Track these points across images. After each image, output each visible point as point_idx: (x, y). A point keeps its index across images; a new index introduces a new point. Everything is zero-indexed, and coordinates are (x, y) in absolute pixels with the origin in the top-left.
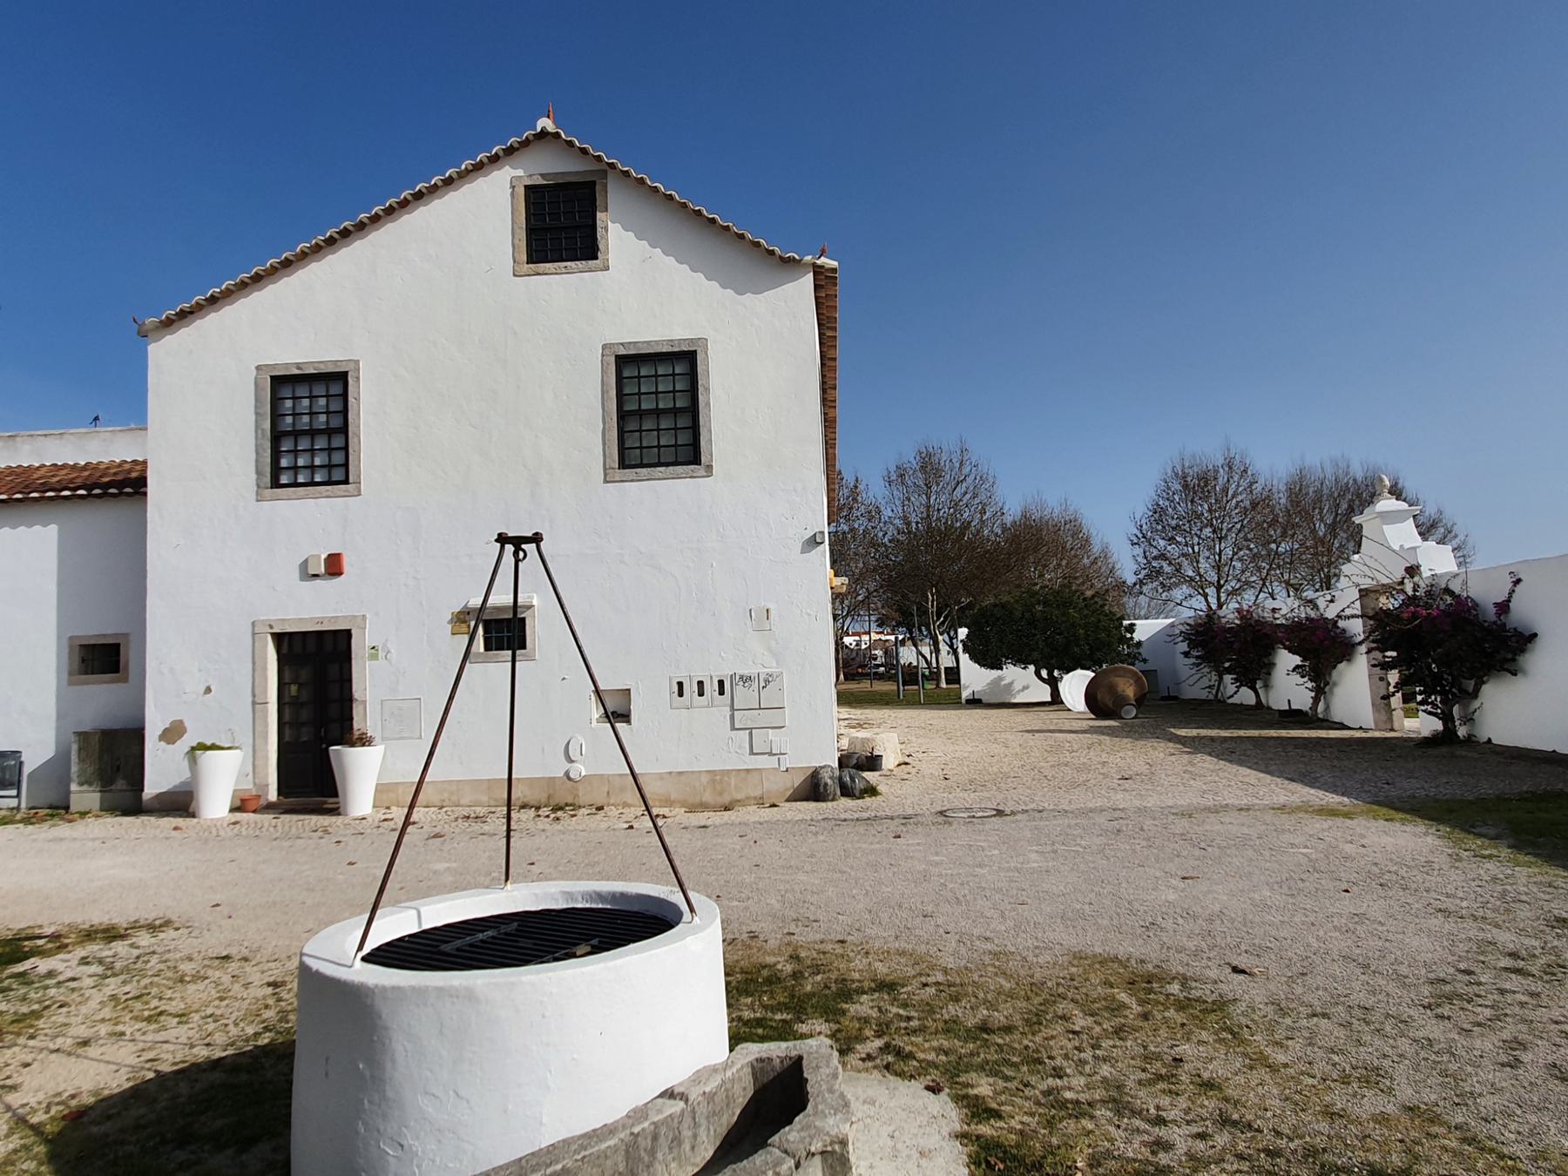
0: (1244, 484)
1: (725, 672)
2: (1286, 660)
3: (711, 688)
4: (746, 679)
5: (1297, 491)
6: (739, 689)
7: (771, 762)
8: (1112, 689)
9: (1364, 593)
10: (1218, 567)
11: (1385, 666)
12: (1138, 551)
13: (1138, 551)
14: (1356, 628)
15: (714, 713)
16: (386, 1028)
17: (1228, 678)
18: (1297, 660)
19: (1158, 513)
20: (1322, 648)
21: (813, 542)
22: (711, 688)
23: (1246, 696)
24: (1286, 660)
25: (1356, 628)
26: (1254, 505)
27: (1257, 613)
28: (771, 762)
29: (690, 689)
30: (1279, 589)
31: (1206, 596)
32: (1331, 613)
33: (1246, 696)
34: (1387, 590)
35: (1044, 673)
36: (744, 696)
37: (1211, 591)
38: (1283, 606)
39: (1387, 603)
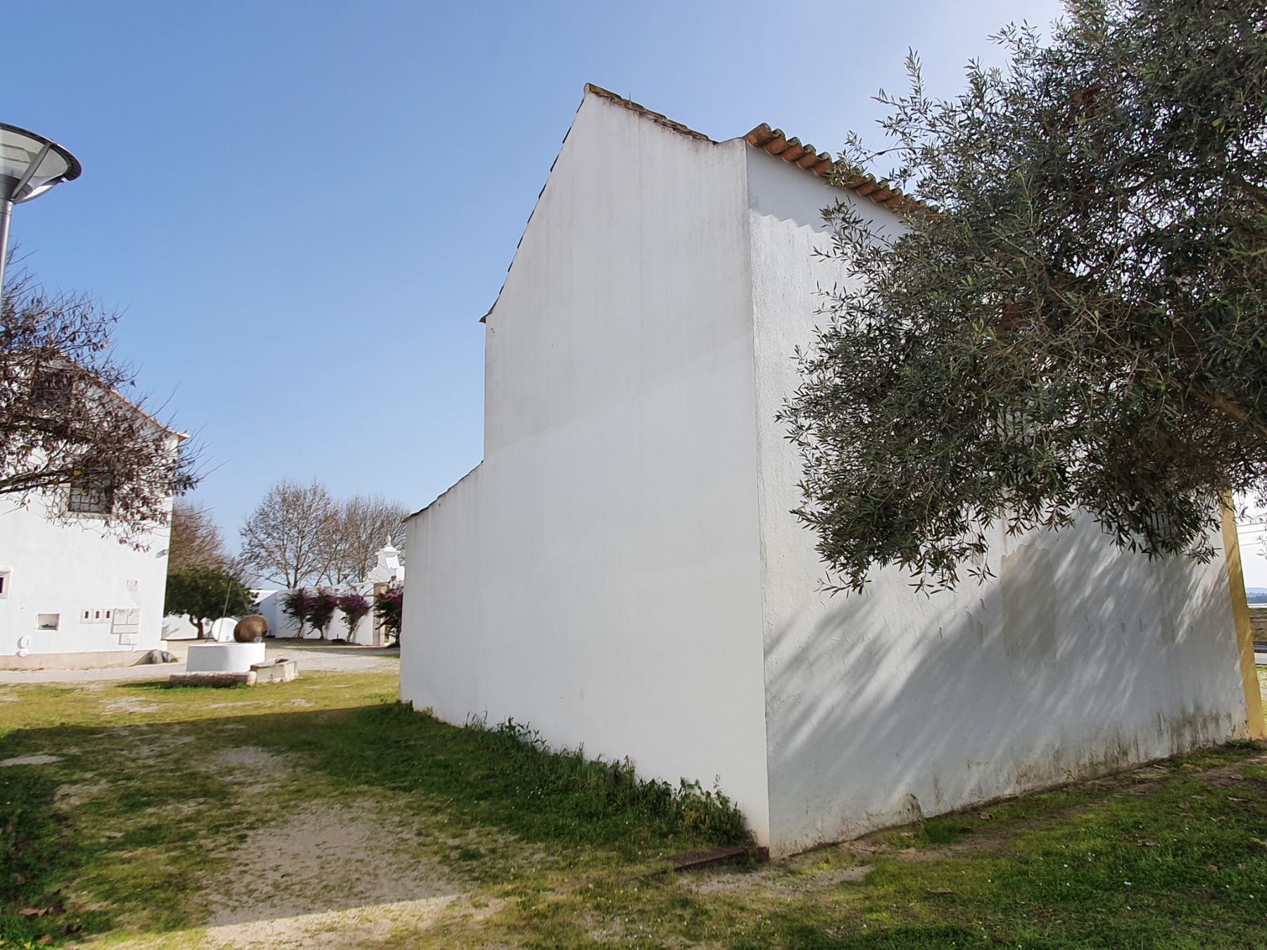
0: (322, 503)
1: (111, 608)
2: (339, 614)
3: (103, 615)
4: (121, 611)
5: (352, 512)
6: (117, 616)
7: (128, 648)
8: (250, 628)
9: (376, 585)
10: (298, 558)
11: (380, 616)
12: (246, 540)
13: (246, 540)
14: (370, 600)
15: (104, 625)
16: (172, 676)
17: (309, 624)
18: (344, 614)
19: (263, 515)
20: (355, 608)
21: (163, 553)
22: (103, 615)
23: (317, 634)
24: (339, 614)
25: (370, 600)
26: (326, 519)
27: (328, 592)
28: (128, 648)
29: (92, 615)
30: (334, 573)
31: (287, 574)
32: (361, 594)
33: (317, 634)
34: (382, 585)
35: (195, 621)
36: (119, 619)
37: (291, 572)
38: (342, 590)
39: (383, 591)
